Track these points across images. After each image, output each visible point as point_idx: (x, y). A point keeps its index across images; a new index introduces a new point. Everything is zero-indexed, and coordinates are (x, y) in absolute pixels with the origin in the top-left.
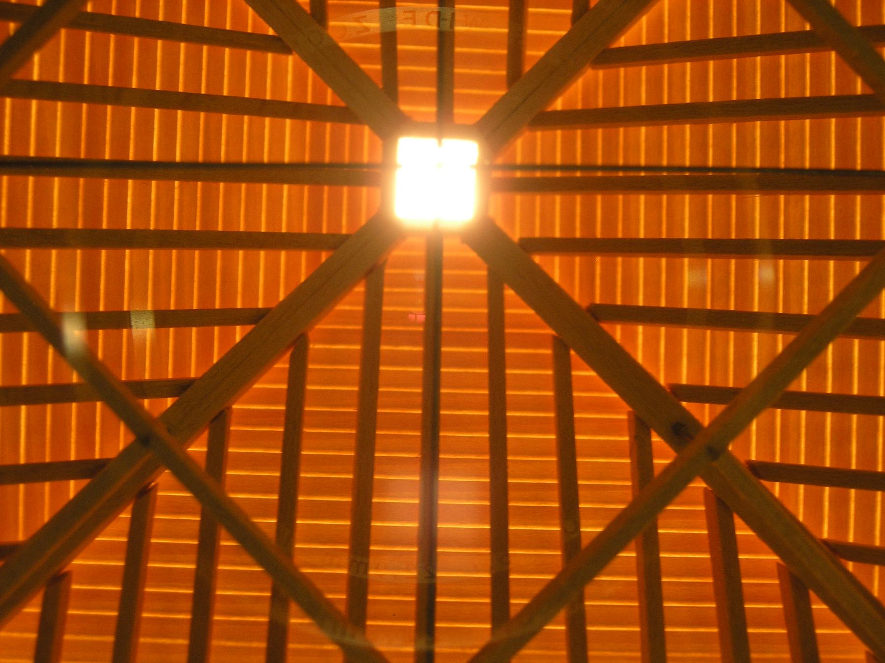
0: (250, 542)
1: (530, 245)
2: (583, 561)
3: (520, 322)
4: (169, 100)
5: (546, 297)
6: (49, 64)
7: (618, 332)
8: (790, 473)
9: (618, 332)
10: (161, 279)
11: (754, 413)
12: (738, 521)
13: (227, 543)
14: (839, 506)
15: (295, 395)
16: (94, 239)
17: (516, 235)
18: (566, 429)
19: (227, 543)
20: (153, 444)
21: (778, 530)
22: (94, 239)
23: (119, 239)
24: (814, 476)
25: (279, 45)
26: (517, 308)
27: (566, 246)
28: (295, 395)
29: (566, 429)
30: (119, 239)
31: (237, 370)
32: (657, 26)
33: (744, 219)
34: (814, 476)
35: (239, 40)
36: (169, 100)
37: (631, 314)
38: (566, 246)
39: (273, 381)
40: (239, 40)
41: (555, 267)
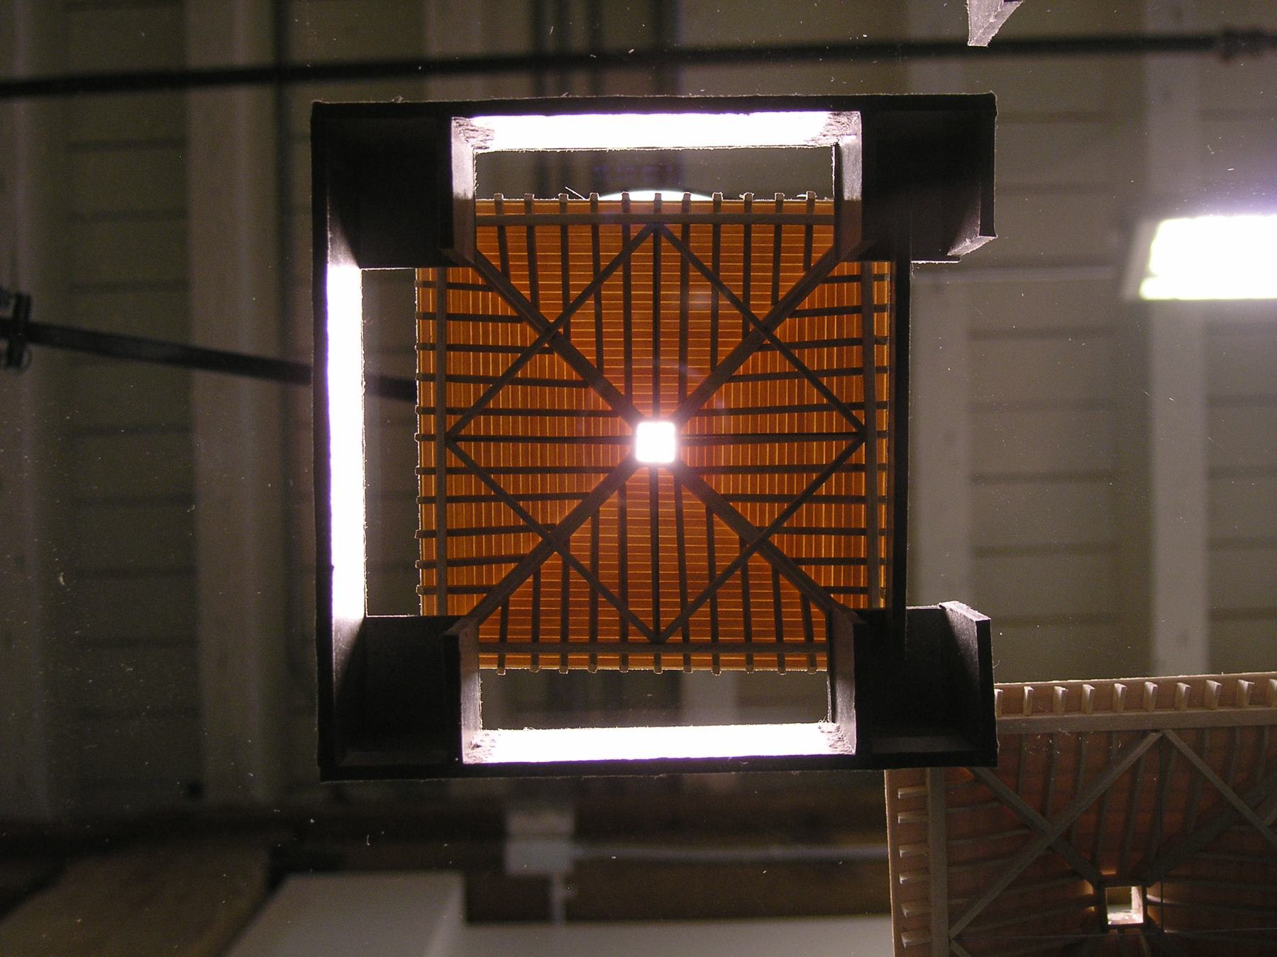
0: (490, 394)
1: (613, 414)
2: (593, 290)
3: (618, 380)
4: (772, 469)
5: (608, 392)
6: (829, 488)
7: (575, 376)
8: (505, 319)
9: (575, 376)
10: (773, 394)
11: (741, 310)
12: (528, 298)
13: (519, 375)
14: (485, 307)
15: (714, 345)
16: (801, 409)
17: (619, 419)
18: (599, 334)
19: (519, 375)
20: (767, 327)
21: (511, 296)
22: (801, 409)
23: (790, 409)
24: (495, 319)
25: (728, 497)
26: (619, 385)
27: (596, 413)
28: (714, 345)
29: (599, 334)
30: (790, 409)
31: (739, 356)
32: (562, 510)
33: (525, 425)
34: (495, 319)
35: (744, 498)
36: (772, 469)
37: (569, 384)
38: (596, 413)
39: (725, 351)
40: (744, 498)
41: (602, 404)
